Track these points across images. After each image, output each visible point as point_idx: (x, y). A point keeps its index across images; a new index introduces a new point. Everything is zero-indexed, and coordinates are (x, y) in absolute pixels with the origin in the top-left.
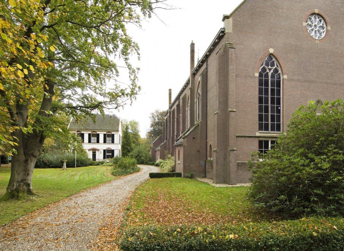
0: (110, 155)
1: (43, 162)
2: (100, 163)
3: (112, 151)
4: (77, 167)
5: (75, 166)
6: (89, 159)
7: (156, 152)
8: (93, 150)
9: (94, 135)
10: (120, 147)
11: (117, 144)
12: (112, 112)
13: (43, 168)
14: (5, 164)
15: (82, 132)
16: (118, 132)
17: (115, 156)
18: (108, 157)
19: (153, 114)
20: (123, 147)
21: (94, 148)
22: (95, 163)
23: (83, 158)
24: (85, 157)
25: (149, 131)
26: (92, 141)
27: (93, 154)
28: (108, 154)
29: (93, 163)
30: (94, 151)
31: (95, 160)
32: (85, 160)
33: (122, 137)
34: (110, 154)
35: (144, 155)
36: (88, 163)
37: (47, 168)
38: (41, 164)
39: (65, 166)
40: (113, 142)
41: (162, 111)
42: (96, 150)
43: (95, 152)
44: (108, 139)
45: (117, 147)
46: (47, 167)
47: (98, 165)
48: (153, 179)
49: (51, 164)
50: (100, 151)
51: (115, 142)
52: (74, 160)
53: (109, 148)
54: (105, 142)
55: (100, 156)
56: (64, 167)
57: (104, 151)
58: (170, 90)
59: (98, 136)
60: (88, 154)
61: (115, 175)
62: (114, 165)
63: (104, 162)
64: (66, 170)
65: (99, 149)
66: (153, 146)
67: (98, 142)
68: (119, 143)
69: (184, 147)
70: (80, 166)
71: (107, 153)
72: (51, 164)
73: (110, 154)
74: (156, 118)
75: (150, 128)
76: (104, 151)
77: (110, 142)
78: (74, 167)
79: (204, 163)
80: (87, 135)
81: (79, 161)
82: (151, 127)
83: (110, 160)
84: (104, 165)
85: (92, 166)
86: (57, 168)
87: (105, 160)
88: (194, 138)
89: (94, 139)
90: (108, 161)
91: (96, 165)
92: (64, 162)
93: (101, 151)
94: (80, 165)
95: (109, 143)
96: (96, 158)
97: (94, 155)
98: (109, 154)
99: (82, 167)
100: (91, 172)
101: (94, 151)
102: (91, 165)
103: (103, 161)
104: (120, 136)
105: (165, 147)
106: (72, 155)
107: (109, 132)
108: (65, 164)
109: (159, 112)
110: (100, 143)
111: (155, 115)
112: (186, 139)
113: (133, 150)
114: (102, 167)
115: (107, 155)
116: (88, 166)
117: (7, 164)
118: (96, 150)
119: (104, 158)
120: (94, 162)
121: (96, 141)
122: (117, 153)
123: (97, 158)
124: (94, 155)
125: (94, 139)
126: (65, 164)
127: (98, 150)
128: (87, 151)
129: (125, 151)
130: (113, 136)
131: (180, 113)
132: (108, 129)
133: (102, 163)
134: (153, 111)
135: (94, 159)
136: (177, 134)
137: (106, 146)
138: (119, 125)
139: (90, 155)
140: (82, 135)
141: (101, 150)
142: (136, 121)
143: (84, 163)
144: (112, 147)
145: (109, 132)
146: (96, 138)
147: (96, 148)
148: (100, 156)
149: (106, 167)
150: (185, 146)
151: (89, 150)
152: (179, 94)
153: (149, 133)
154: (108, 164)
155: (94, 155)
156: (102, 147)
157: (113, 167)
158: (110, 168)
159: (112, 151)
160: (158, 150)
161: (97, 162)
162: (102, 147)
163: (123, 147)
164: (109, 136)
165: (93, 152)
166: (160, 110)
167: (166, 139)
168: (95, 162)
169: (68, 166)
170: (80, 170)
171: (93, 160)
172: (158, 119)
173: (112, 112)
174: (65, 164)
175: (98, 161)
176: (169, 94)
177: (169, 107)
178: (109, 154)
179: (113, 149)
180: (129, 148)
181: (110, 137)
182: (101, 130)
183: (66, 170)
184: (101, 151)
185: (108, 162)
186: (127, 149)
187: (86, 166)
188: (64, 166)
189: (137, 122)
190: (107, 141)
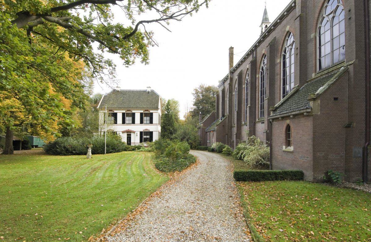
0: (147, 138)
1: (65, 147)
2: (136, 147)
3: (151, 134)
4: (107, 153)
5: (104, 152)
6: (123, 143)
7: (208, 133)
8: (127, 132)
9: (146, 115)
10: (159, 128)
11: (156, 124)
12: (149, 87)
13: (65, 155)
14: (27, 149)
15: (115, 111)
16: (157, 110)
17: (154, 140)
18: (146, 140)
19: (196, 90)
20: (164, 128)
21: (129, 130)
22: (129, 148)
23: (116, 142)
24: (117, 140)
25: (192, 110)
26: (127, 122)
27: (128, 137)
28: (145, 137)
29: (128, 148)
30: (129, 134)
31: (130, 144)
32: (118, 144)
33: (162, 117)
34: (148, 137)
35: (192, 137)
36: (121, 148)
37: (69, 155)
38: (62, 150)
39: (90, 153)
40: (151, 122)
41: (207, 86)
42: (131, 132)
43: (130, 135)
44: (145, 118)
45: (156, 129)
46: (70, 154)
47: (133, 150)
48: (242, 184)
49: (75, 150)
50: (136, 133)
51: (154, 122)
52: (104, 144)
53: (146, 130)
54: (142, 122)
55: (136, 140)
56: (89, 154)
57: (141, 133)
58: (231, 49)
59: (133, 115)
60: (122, 137)
61: (162, 171)
62: (155, 151)
63: (141, 146)
64: (92, 158)
65: (135, 130)
66: (203, 126)
67: (133, 122)
68: (159, 124)
69: (315, 118)
70: (111, 152)
71: (144, 135)
72: (75, 150)
73: (148, 137)
74: (200, 95)
75: (192, 106)
76: (141, 133)
77: (148, 122)
78: (104, 153)
79: (361, 150)
80: (139, 114)
81: (109, 145)
82: (194, 105)
83: (148, 144)
84: (142, 151)
85: (126, 152)
86: (82, 155)
87: (142, 144)
88: (336, 99)
89: (128, 119)
90: (145, 145)
91: (131, 151)
92: (88, 148)
93: (137, 133)
94: (111, 150)
95: (147, 124)
96: (131, 142)
97: (129, 138)
98: (146, 136)
99: (114, 152)
100: (125, 162)
101: (129, 134)
102: (125, 150)
103: (140, 145)
104: (159, 115)
105: (223, 126)
106: (102, 138)
107: (146, 110)
108: (90, 151)
109: (205, 87)
110: (135, 123)
111: (200, 91)
112: (319, 101)
113: (176, 131)
114: (139, 153)
115: (144, 138)
116: (121, 151)
117: (29, 149)
118: (131, 132)
119: (141, 141)
120: (128, 147)
121: (131, 122)
122: (156, 137)
123: (132, 141)
124: (129, 138)
125: (128, 119)
126: (90, 151)
127: (134, 132)
128: (121, 134)
129: (166, 133)
130: (151, 115)
131: (256, 73)
132: (145, 107)
133: (139, 148)
134: (197, 86)
135: (129, 143)
136: (251, 104)
137: (143, 128)
138: (158, 102)
139: (124, 139)
140: (115, 115)
141: (137, 132)
142: (176, 99)
143: (116, 148)
144: (150, 128)
145: (146, 110)
146: (131, 118)
147: (131, 130)
148: (136, 140)
149: (144, 152)
150: (317, 115)
151: (123, 132)
152: (252, 49)
153: (191, 112)
154: (146, 149)
155: (128, 138)
156: (138, 128)
157: (153, 154)
158: (149, 155)
159: (151, 134)
160: (213, 131)
161: (132, 146)
162: (138, 128)
163: (164, 128)
164: (146, 115)
165: (128, 135)
166: (206, 85)
167: (223, 116)
168: (129, 146)
169: (93, 153)
170: (110, 159)
171: (128, 144)
172: (203, 96)
173: (149, 87)
174: (91, 151)
175: (134, 145)
176: (230, 54)
177: (230, 71)
178: (146, 136)
179: (151, 130)
180: (171, 129)
181: (147, 116)
182: (137, 108)
183: (92, 158)
184: (137, 133)
185: (145, 147)
186: (169, 130)
187: (119, 152)
188: (88, 153)
189: (177, 101)
190: (145, 122)
